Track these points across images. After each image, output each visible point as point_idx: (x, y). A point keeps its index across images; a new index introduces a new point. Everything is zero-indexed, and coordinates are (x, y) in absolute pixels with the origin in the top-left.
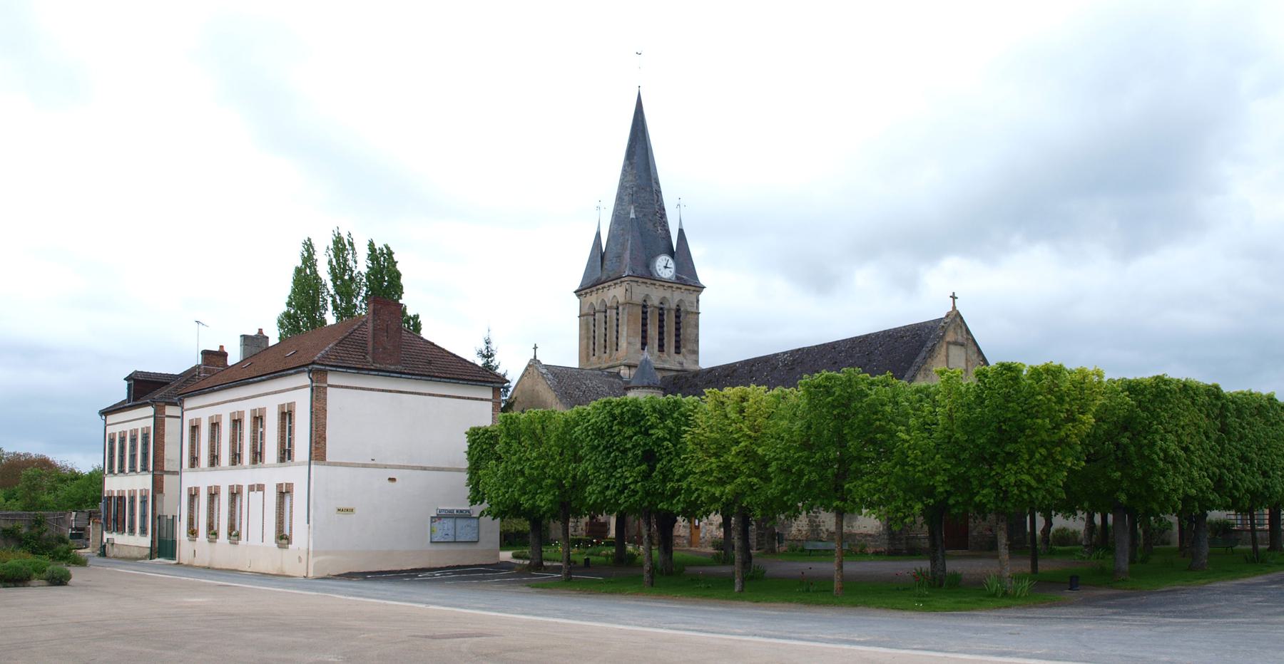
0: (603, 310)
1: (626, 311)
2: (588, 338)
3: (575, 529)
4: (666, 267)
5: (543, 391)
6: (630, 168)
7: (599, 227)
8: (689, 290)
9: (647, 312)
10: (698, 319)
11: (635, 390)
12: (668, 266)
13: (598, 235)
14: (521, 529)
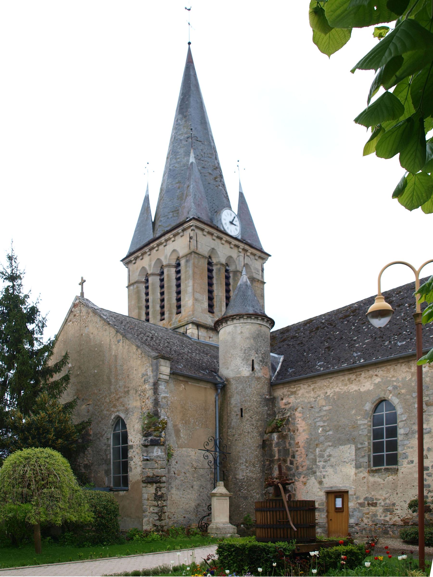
0: (158, 272)
1: (191, 263)
2: (140, 308)
3: (160, 516)
4: (231, 223)
5: (96, 332)
6: (183, 121)
7: (147, 191)
8: (255, 255)
9: (213, 270)
10: (263, 289)
11: (235, 321)
12: (234, 222)
13: (147, 199)
14: (74, 519)
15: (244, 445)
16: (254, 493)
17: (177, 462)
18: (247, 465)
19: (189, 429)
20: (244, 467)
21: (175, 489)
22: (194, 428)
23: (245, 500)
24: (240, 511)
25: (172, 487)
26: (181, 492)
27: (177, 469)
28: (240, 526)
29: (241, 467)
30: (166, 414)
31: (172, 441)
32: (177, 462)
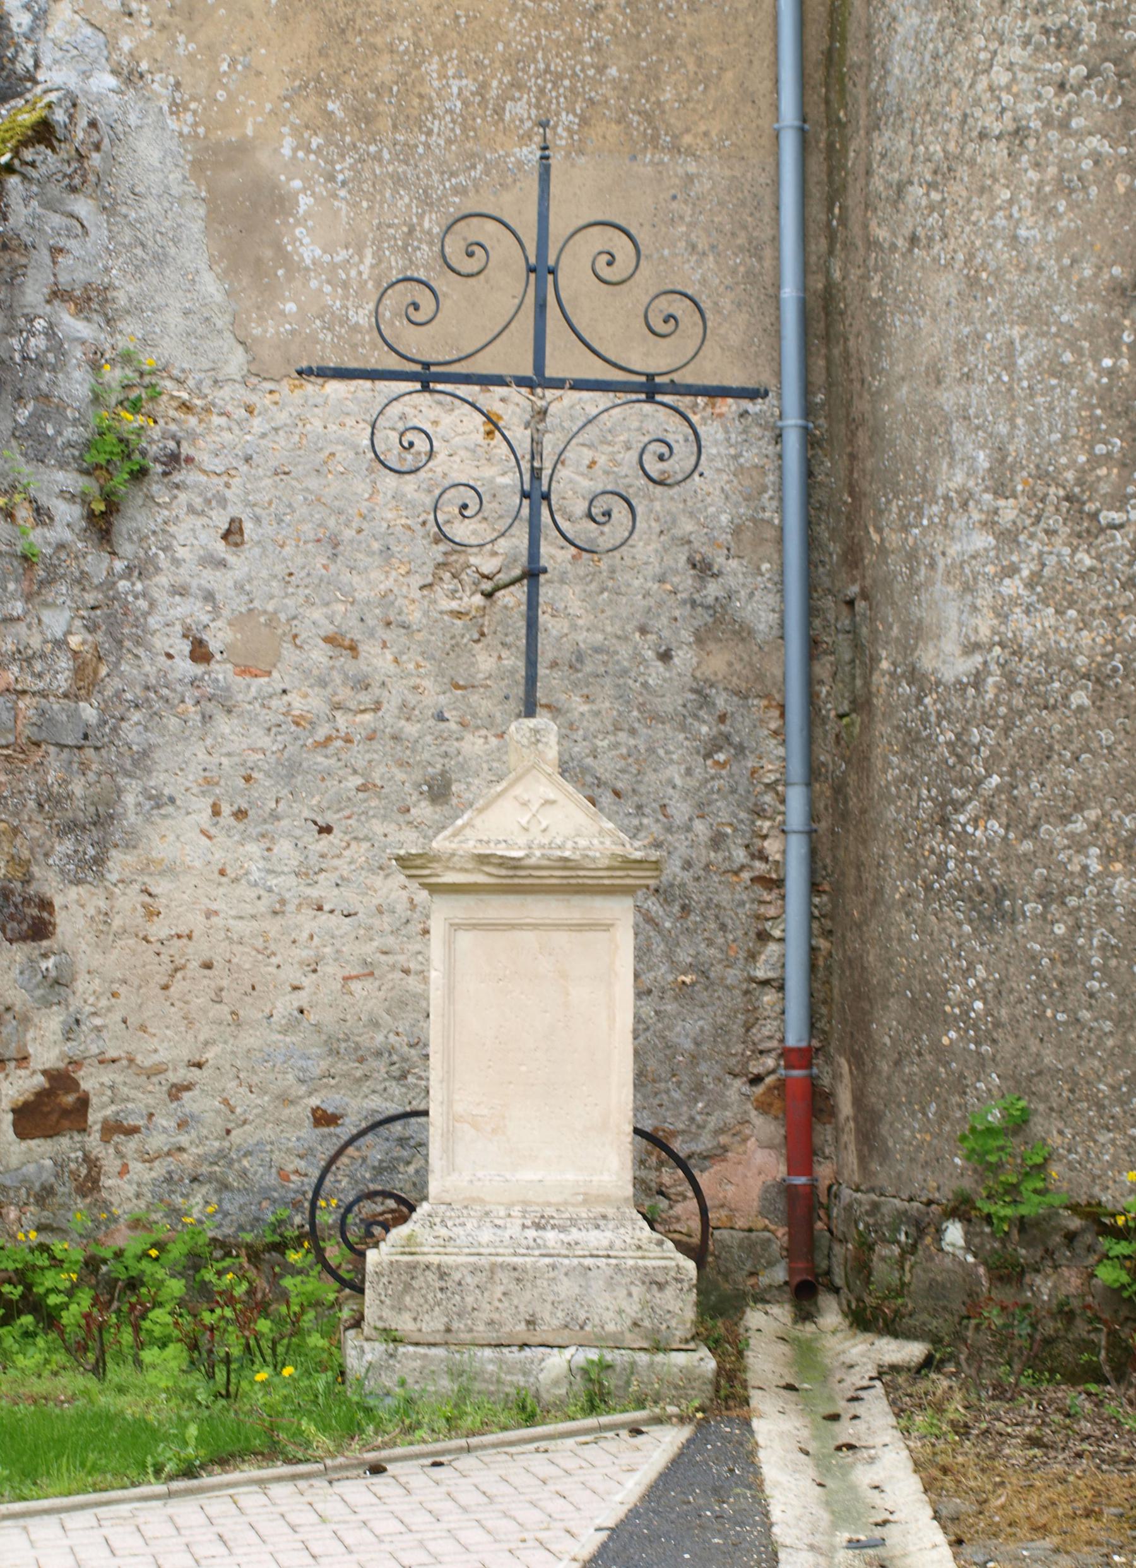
15: (973, 282)
16: (1079, 845)
17: (232, 533)
18: (1008, 510)
19: (399, 181)
20: (983, 541)
21: (204, 817)
22: (472, 158)
23: (986, 923)
24: (938, 1050)
25: (158, 801)
26: (284, 847)
27: (239, 604)
28: (940, 1232)
29: (954, 549)
30: (111, 44)
31: (173, 318)
32: (232, 533)
